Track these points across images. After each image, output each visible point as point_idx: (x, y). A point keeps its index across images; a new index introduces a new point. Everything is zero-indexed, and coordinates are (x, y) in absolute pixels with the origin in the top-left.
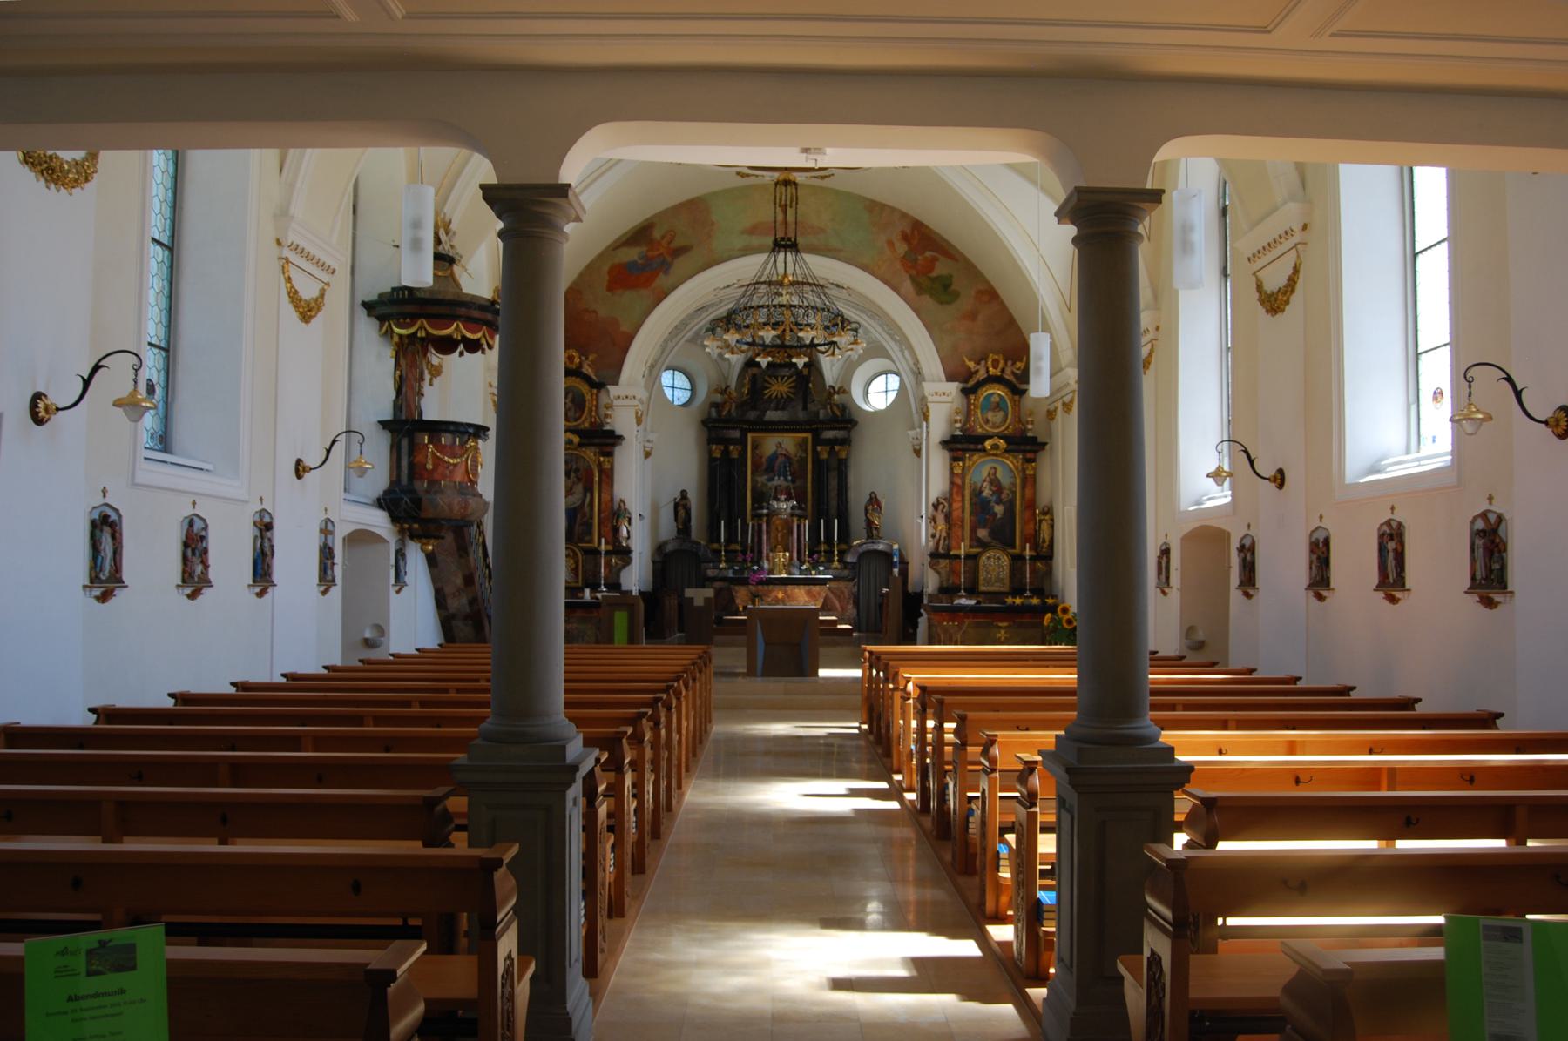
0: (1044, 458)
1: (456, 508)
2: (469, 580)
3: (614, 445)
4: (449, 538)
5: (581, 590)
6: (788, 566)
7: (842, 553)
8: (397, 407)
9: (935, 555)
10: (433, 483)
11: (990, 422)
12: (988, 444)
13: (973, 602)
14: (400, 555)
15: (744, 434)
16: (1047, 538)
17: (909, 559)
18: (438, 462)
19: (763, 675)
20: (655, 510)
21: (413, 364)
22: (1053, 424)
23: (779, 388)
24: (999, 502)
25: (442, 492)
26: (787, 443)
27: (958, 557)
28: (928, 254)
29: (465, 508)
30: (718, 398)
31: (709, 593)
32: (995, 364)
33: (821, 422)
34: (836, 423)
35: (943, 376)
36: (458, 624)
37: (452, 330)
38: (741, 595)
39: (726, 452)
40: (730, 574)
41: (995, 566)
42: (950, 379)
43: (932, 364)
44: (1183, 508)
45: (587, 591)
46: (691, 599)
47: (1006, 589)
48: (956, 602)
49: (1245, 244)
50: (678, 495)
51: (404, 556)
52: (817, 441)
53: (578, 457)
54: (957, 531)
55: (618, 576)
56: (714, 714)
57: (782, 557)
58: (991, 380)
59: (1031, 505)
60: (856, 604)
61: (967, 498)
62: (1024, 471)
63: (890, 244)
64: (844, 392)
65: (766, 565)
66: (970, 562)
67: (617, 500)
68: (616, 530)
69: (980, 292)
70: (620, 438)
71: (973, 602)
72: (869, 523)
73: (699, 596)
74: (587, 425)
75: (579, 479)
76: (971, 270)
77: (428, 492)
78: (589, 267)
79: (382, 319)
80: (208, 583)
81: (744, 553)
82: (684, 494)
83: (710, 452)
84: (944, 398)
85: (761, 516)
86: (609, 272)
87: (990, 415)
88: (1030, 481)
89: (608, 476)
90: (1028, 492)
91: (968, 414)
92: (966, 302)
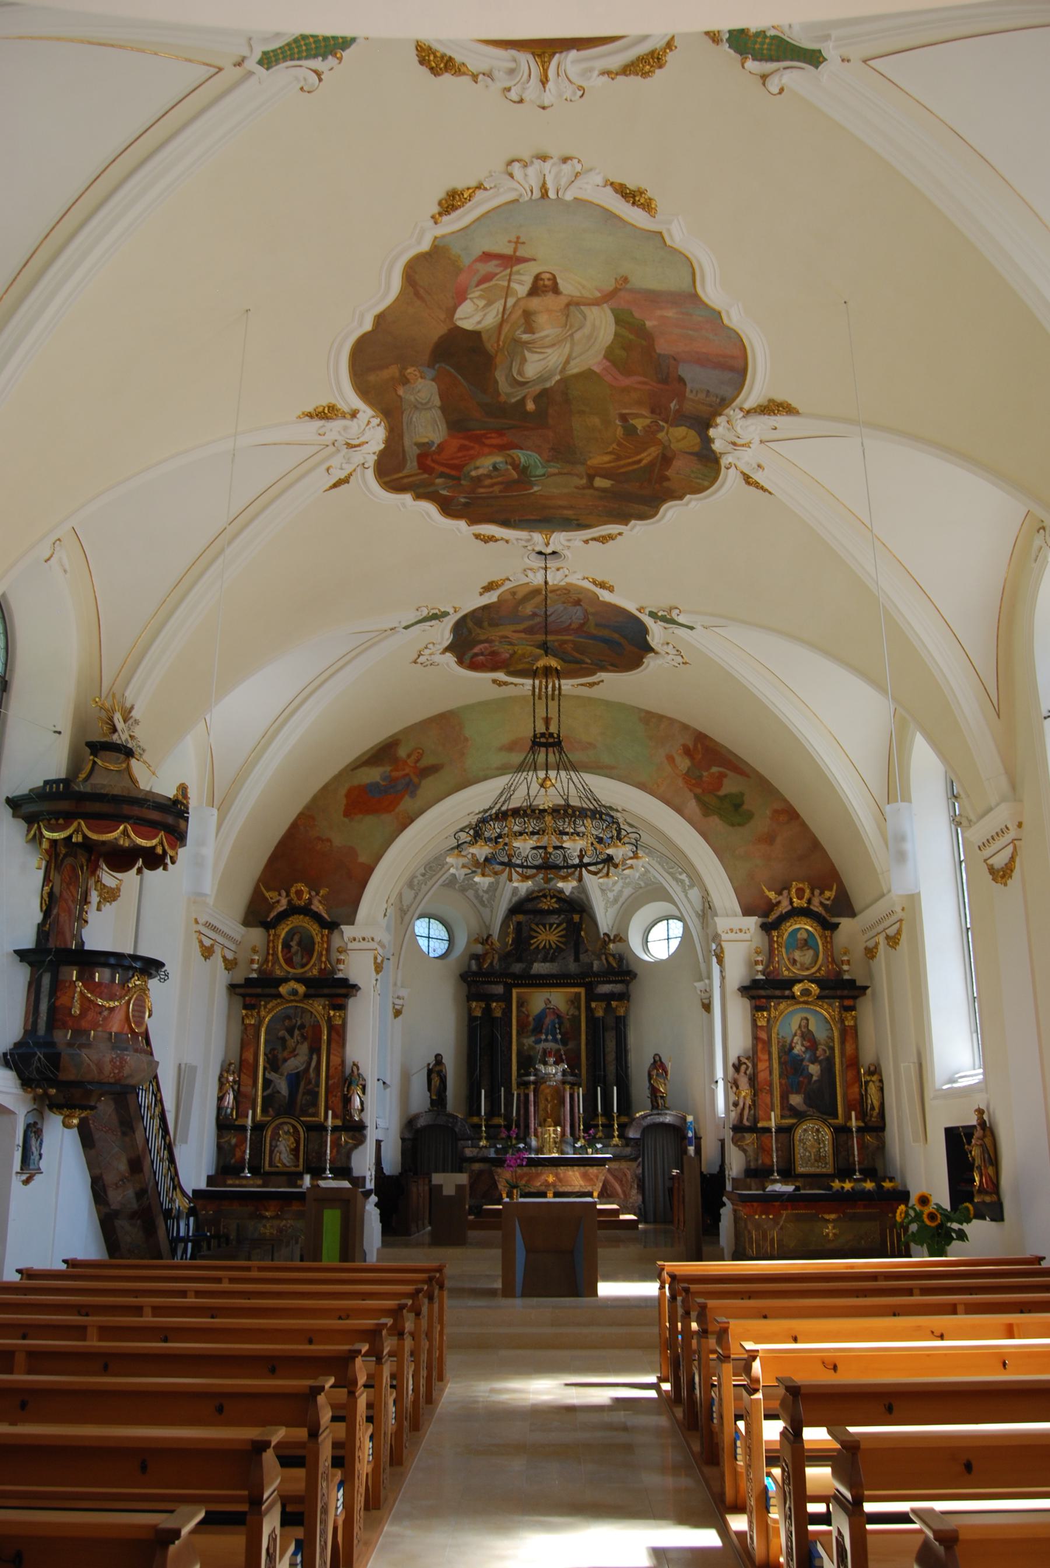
0: (865, 1006)
1: (108, 1068)
2: (136, 1165)
3: (347, 996)
4: (106, 1108)
5: (300, 1176)
6: (560, 1144)
7: (622, 1127)
8: (43, 932)
9: (738, 1129)
10: (80, 1033)
11: (794, 963)
12: (797, 989)
13: (790, 1188)
14: (33, 1131)
15: (508, 989)
16: (876, 1104)
17: (702, 1134)
18: (87, 1005)
19: (524, 1295)
20: (406, 1078)
21: (73, 880)
22: (874, 963)
23: (548, 937)
24: (814, 1060)
25: (88, 1045)
26: (558, 998)
27: (768, 1130)
28: (714, 769)
29: (121, 1068)
30: (479, 949)
31: (463, 1178)
32: (800, 893)
33: (596, 975)
34: (609, 977)
35: (738, 910)
36: (123, 1224)
37: (118, 835)
38: (504, 1176)
39: (487, 1010)
41: (813, 1140)
42: (747, 912)
43: (724, 895)
44: (937, 1086)
45: (307, 1180)
46: (441, 1186)
47: (829, 1169)
50: (432, 1060)
51: (39, 1133)
52: (591, 996)
56: (451, 1360)
57: (552, 1132)
59: (853, 1063)
60: (641, 1188)
61: (775, 1055)
63: (671, 759)
64: (621, 940)
65: (534, 1143)
66: (782, 1135)
67: (349, 1063)
68: (347, 1100)
69: (776, 811)
70: (355, 987)
71: (790, 1188)
72: (654, 1091)
74: (315, 972)
75: (304, 1038)
77: (70, 1045)
78: (325, 788)
79: (30, 820)
81: (508, 1127)
83: (470, 1010)
84: (741, 936)
85: (526, 1084)
86: (348, 795)
87: (797, 955)
88: (850, 1034)
89: (339, 1034)
90: (849, 1048)
91: (771, 951)
92: (761, 823)
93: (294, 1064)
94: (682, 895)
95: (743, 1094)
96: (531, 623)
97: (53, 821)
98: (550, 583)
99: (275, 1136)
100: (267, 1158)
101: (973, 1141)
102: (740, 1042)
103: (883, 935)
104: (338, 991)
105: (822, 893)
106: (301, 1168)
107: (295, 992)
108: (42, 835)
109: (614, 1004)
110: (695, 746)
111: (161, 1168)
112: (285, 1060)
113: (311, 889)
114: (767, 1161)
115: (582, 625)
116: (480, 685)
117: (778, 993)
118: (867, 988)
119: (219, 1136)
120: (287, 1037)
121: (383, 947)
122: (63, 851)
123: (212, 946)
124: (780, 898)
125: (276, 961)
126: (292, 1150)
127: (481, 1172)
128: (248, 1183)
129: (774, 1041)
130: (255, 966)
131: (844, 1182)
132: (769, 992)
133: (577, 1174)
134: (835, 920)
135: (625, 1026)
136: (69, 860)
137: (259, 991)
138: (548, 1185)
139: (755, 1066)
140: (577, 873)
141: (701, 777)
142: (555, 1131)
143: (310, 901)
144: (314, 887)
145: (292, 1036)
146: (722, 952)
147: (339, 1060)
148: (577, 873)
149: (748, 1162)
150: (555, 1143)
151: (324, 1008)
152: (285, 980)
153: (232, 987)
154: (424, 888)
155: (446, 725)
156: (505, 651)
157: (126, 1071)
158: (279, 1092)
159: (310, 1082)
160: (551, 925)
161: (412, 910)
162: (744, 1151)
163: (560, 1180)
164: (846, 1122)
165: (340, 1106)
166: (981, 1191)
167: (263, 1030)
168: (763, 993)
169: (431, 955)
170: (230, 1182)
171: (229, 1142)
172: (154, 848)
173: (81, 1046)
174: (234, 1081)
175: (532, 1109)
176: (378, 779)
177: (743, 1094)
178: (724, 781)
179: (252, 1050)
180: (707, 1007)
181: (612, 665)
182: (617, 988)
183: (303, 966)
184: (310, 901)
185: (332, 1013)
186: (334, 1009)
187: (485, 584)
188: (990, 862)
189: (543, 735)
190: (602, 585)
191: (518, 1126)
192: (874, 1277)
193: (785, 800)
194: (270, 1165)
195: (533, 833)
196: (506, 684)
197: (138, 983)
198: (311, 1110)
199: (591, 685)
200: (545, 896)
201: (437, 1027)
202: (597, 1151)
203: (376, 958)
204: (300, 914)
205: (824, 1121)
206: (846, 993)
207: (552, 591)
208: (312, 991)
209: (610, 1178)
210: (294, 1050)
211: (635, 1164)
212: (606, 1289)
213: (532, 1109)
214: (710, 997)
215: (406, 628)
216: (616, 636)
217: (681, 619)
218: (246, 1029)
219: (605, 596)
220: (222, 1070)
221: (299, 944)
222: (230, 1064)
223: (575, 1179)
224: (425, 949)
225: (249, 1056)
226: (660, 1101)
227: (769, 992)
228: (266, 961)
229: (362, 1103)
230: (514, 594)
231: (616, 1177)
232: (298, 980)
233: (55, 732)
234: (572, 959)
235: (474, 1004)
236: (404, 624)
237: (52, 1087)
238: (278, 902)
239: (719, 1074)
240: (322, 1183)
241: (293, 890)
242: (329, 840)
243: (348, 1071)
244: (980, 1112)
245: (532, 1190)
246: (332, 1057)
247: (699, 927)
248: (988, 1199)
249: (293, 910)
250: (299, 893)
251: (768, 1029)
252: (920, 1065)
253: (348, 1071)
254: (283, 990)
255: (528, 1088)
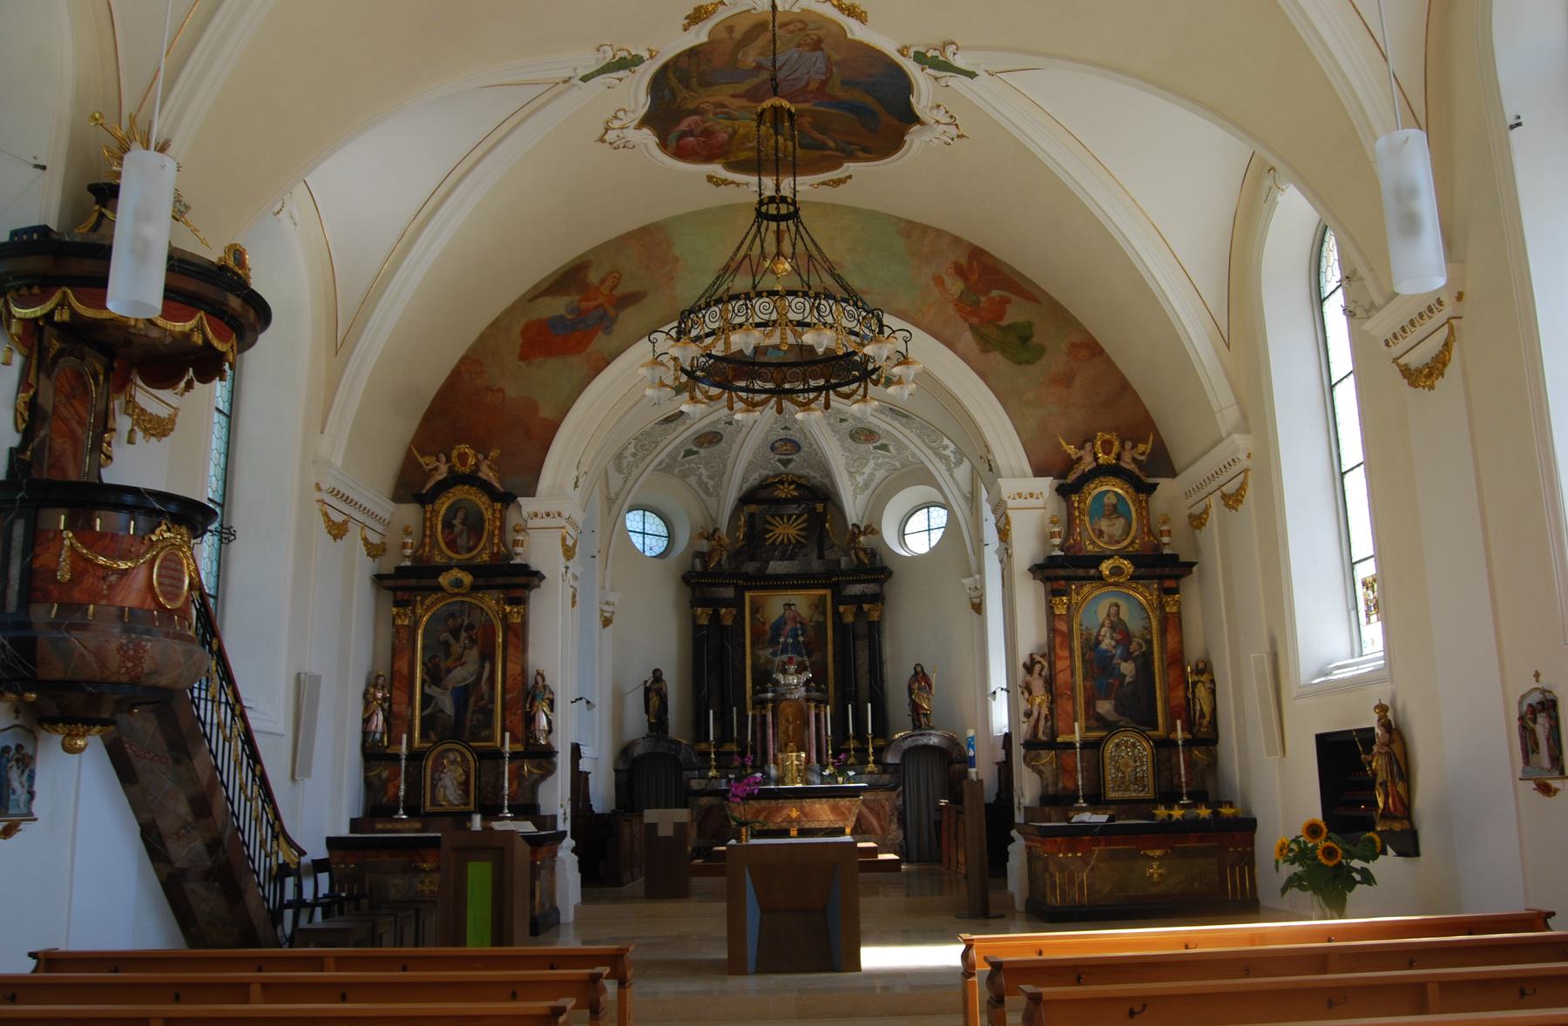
0: (1190, 588)
1: (114, 660)
3: (528, 587)
5: (467, 816)
7: (879, 751)
9: (1032, 745)
10: (71, 608)
11: (1105, 534)
12: (1105, 567)
13: (1102, 818)
15: (740, 592)
18: (82, 567)
20: (619, 698)
22: (1202, 535)
23: (786, 530)
25: (84, 627)
26: (801, 601)
27: (1071, 745)
28: (995, 293)
30: (704, 546)
31: (683, 815)
33: (844, 573)
34: (863, 574)
35: (1028, 470)
36: (195, 889)
39: (716, 617)
40: (723, 785)
41: (1129, 756)
42: (1039, 472)
43: (1008, 448)
45: (477, 822)
46: (654, 826)
48: (1076, 819)
49: (1381, 325)
50: (649, 677)
52: (839, 599)
53: (472, 607)
54: (1065, 705)
55: (534, 793)
57: (795, 759)
58: (1100, 471)
59: (1177, 659)
62: (1162, 606)
63: (939, 280)
65: (773, 772)
66: (1088, 752)
67: (532, 673)
68: (530, 719)
69: (1074, 345)
70: (539, 576)
71: (1102, 818)
72: (916, 708)
73: (666, 819)
74: (485, 557)
76: (1060, 315)
77: (54, 625)
78: (495, 325)
80: (30, 817)
81: (742, 754)
82: (657, 674)
83: (694, 618)
84: (1032, 502)
85: (766, 701)
86: (524, 333)
87: (1104, 525)
88: (1172, 623)
89: (518, 635)
90: (1171, 640)
92: (1056, 359)
93: (461, 675)
94: (946, 474)
95: (1038, 700)
96: (756, 80)
97: (24, 291)
98: (780, 9)
99: (438, 767)
100: (428, 795)
101: (1375, 748)
102: (1031, 636)
103: (1219, 493)
104: (518, 581)
105: (1134, 446)
106: (472, 807)
107: (458, 583)
108: (10, 315)
109: (866, 607)
110: (970, 263)
111: (246, 811)
112: (449, 670)
113: (477, 451)
114: (1070, 785)
115: (824, 83)
116: (690, 185)
117: (1081, 572)
118: (1194, 564)
119: (367, 769)
120: (452, 641)
121: (575, 526)
122: (56, 345)
123: (345, 522)
124: (1082, 453)
125: (435, 544)
126: (460, 784)
127: (711, 807)
128: (404, 827)
129: (1076, 634)
130: (409, 552)
131: (1172, 808)
132: (1069, 572)
133: (826, 807)
134: (1152, 481)
135: (879, 633)
136: (67, 363)
137: (413, 582)
138: (790, 821)
139: (1052, 665)
140: (822, 399)
141: (978, 302)
142: (798, 757)
143: (477, 466)
144: (482, 448)
145: (457, 639)
146: (1008, 523)
147: (518, 669)
148: (822, 399)
149: (1044, 787)
150: (799, 771)
151: (498, 603)
152: (447, 568)
153: (379, 579)
154: (636, 472)
155: (650, 240)
156: (722, 129)
157: (147, 665)
158: (442, 711)
159: (482, 698)
160: (790, 517)
161: (621, 498)
162: (1040, 773)
163: (805, 815)
164: (1169, 733)
165: (522, 726)
166: (1387, 815)
167: (420, 632)
168: (1062, 572)
169: (648, 553)
170: (379, 826)
171: (379, 776)
172: (187, 336)
173: (72, 627)
174: (384, 699)
175: (770, 731)
176: (562, 311)
177: (1038, 700)
178: (1003, 307)
179: (406, 659)
180: (978, 607)
181: (864, 150)
182: (869, 588)
183: (470, 550)
184: (477, 466)
185: (508, 609)
186: (510, 604)
187: (690, 11)
188: (1402, 361)
189: (772, 200)
190: (851, 11)
191: (754, 752)
192: (1319, 960)
193: (1087, 332)
194: (433, 803)
195: (758, 325)
196: (725, 182)
197: (167, 535)
198: (485, 733)
199: (837, 183)
200: (781, 482)
201: (656, 638)
202: (849, 780)
203: (564, 539)
204: (464, 483)
205: (1142, 733)
206: (1167, 571)
207: (783, 25)
208: (481, 581)
209: (866, 812)
210: (461, 656)
211: (894, 794)
212: (874, 957)
213: (770, 731)
214: (982, 596)
215: (585, 79)
216: (869, 100)
217: (959, 61)
218: (397, 632)
219: (857, 31)
220: (368, 684)
221: (464, 522)
222: (378, 677)
223: (823, 813)
224: (640, 547)
225: (403, 666)
226: (923, 720)
227: (1069, 572)
228: (422, 545)
229: (549, 722)
230: (730, 29)
231: (870, 809)
232: (462, 568)
233: (36, 166)
234: (815, 556)
235: (699, 610)
236: (582, 72)
237: (31, 691)
238: (436, 469)
239: (998, 677)
240: (497, 825)
241: (455, 453)
242: (501, 390)
243: (531, 683)
244: (1382, 709)
245: (772, 827)
246: (509, 665)
247: (967, 512)
248: (1397, 826)
249: (454, 479)
250: (463, 457)
251: (1068, 618)
252: (1275, 657)
253: (531, 683)
254: (444, 580)
255: (765, 708)
